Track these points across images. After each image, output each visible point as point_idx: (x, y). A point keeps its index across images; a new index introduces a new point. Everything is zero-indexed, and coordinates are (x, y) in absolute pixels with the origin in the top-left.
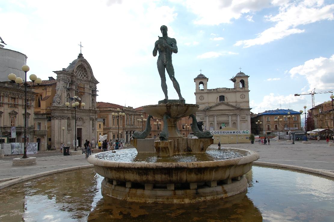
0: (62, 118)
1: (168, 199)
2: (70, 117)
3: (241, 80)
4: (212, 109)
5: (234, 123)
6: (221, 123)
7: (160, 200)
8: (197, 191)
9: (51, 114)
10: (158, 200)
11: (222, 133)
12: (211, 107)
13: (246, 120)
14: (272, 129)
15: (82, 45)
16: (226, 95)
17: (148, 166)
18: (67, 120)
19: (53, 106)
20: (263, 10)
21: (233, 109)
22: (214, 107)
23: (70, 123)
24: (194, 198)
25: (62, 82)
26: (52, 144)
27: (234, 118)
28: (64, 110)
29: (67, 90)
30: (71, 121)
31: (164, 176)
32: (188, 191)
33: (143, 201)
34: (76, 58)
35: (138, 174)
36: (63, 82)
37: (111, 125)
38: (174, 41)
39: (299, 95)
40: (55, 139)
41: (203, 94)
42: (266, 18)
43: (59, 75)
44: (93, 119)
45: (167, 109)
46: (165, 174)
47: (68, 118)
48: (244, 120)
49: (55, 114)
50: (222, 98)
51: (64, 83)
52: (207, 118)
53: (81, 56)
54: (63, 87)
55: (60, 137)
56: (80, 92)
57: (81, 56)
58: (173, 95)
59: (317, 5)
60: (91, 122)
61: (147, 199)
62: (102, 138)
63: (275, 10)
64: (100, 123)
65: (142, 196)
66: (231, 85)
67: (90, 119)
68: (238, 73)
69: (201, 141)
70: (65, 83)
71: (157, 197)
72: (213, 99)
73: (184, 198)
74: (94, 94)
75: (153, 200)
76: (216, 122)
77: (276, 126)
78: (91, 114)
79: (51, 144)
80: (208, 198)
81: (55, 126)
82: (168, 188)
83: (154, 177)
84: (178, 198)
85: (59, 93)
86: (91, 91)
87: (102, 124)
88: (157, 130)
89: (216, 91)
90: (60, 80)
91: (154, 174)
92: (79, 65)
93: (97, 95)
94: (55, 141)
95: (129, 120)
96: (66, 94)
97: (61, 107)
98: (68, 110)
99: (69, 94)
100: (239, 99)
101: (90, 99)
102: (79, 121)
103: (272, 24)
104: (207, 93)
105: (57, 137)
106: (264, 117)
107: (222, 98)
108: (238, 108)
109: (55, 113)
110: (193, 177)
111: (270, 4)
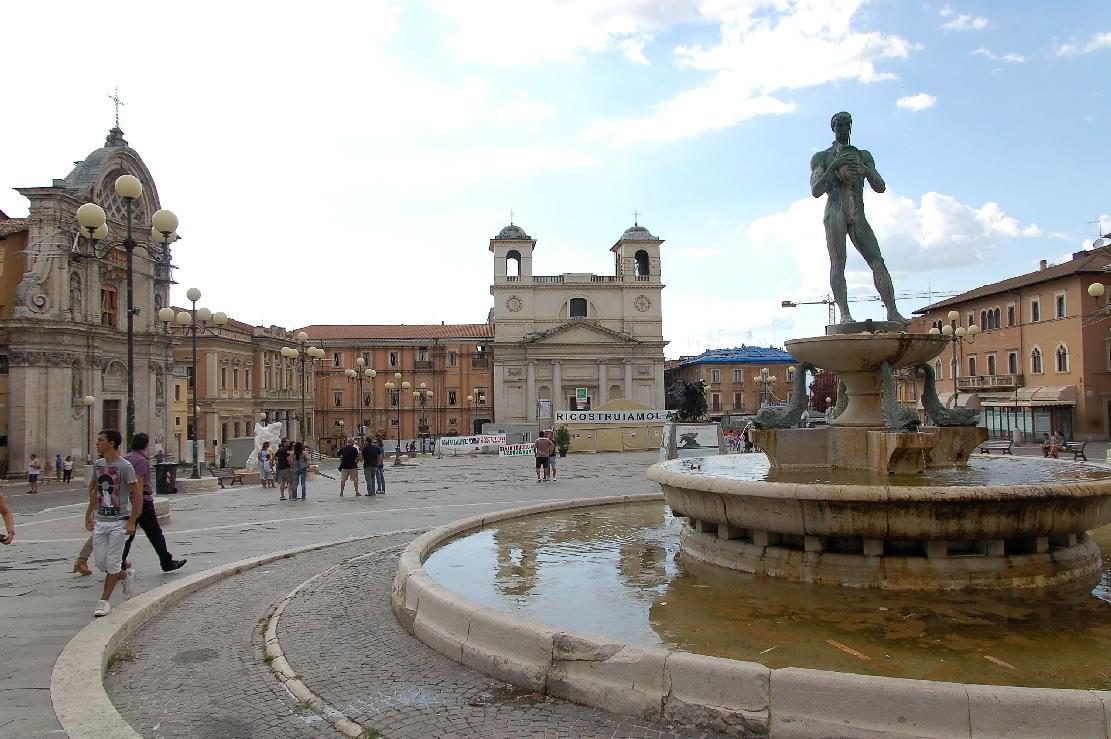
0: (53, 361)
1: (999, 578)
2: (82, 357)
3: (640, 255)
4: (546, 342)
5: (616, 390)
6: (573, 388)
7: (981, 581)
8: (1052, 557)
9: (6, 346)
10: (976, 581)
11: (603, 417)
12: (544, 336)
13: (650, 379)
14: (729, 408)
15: (120, 100)
16: (592, 297)
17: (979, 494)
18: (69, 371)
19: (17, 316)
20: (678, 26)
21: (610, 340)
22: (554, 333)
23: (81, 382)
24: (1054, 574)
25: (50, 231)
26: (11, 455)
27: (615, 372)
28: (62, 332)
29: (69, 263)
30: (84, 373)
31: (1004, 520)
32: (1035, 557)
33: (933, 586)
34: (100, 142)
35: (934, 517)
36: (58, 231)
37: (213, 387)
38: (866, 158)
39: (794, 305)
40: (27, 440)
41: (648, 290)
42: (682, 57)
43: (38, 204)
44: (160, 368)
45: (901, 346)
46: (1008, 514)
47: (76, 363)
48: (646, 377)
49: (27, 346)
50: (579, 307)
51: (61, 233)
52: (531, 369)
53: (116, 136)
54: (58, 246)
55: (43, 432)
56: (116, 269)
57: (116, 136)
58: (866, 307)
59: (829, 31)
60: (153, 377)
61: (945, 581)
62: (268, 433)
63: (711, 33)
64: (178, 382)
65: (929, 574)
66: (606, 267)
67: (150, 367)
68: (631, 230)
69: (956, 433)
70: (64, 233)
71: (972, 575)
72: (552, 309)
73: (1034, 575)
74: (163, 277)
75: (962, 582)
76: (558, 384)
77: (738, 397)
78: (153, 350)
79: (7, 456)
80: (1077, 573)
81: (27, 391)
82: (991, 552)
83: (981, 523)
84: (1021, 576)
85: (38, 268)
86: (152, 265)
87: (184, 385)
88: (448, 406)
89: (561, 282)
90: (41, 221)
91: (980, 515)
92: (110, 173)
93: (174, 283)
94: (26, 447)
95: (274, 370)
96: (66, 276)
97: (49, 321)
98: (75, 333)
99: (75, 273)
100: (631, 313)
101: (148, 296)
102: (112, 373)
103: (696, 78)
104: (535, 288)
105: (34, 432)
106: (703, 370)
107: (579, 307)
108: (629, 340)
109: (24, 343)
110: (991, 523)
111: (696, 12)
